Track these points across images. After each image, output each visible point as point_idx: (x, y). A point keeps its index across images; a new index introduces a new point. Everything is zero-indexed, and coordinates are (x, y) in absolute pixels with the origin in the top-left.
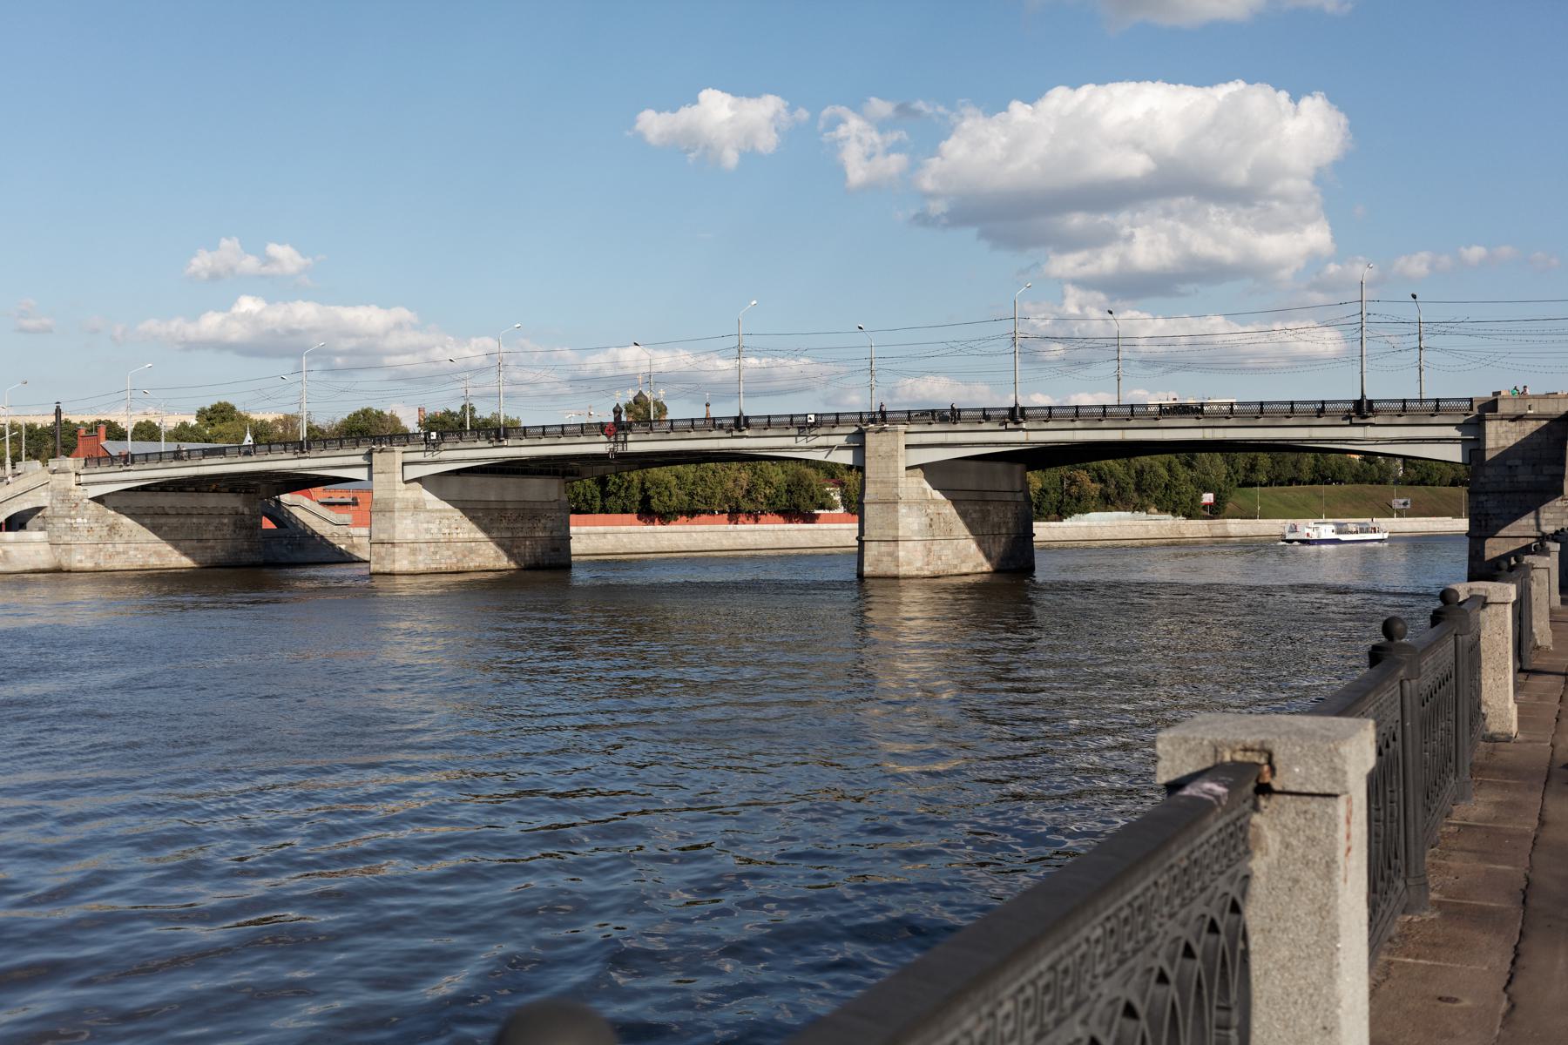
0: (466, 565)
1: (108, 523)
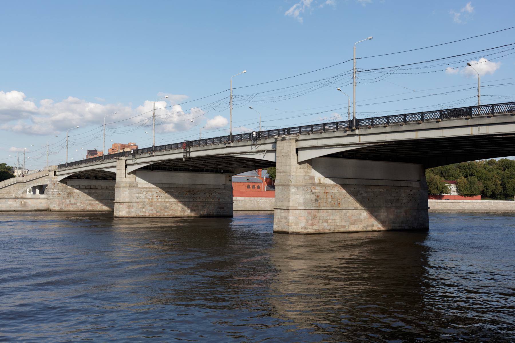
1: (68, 192)
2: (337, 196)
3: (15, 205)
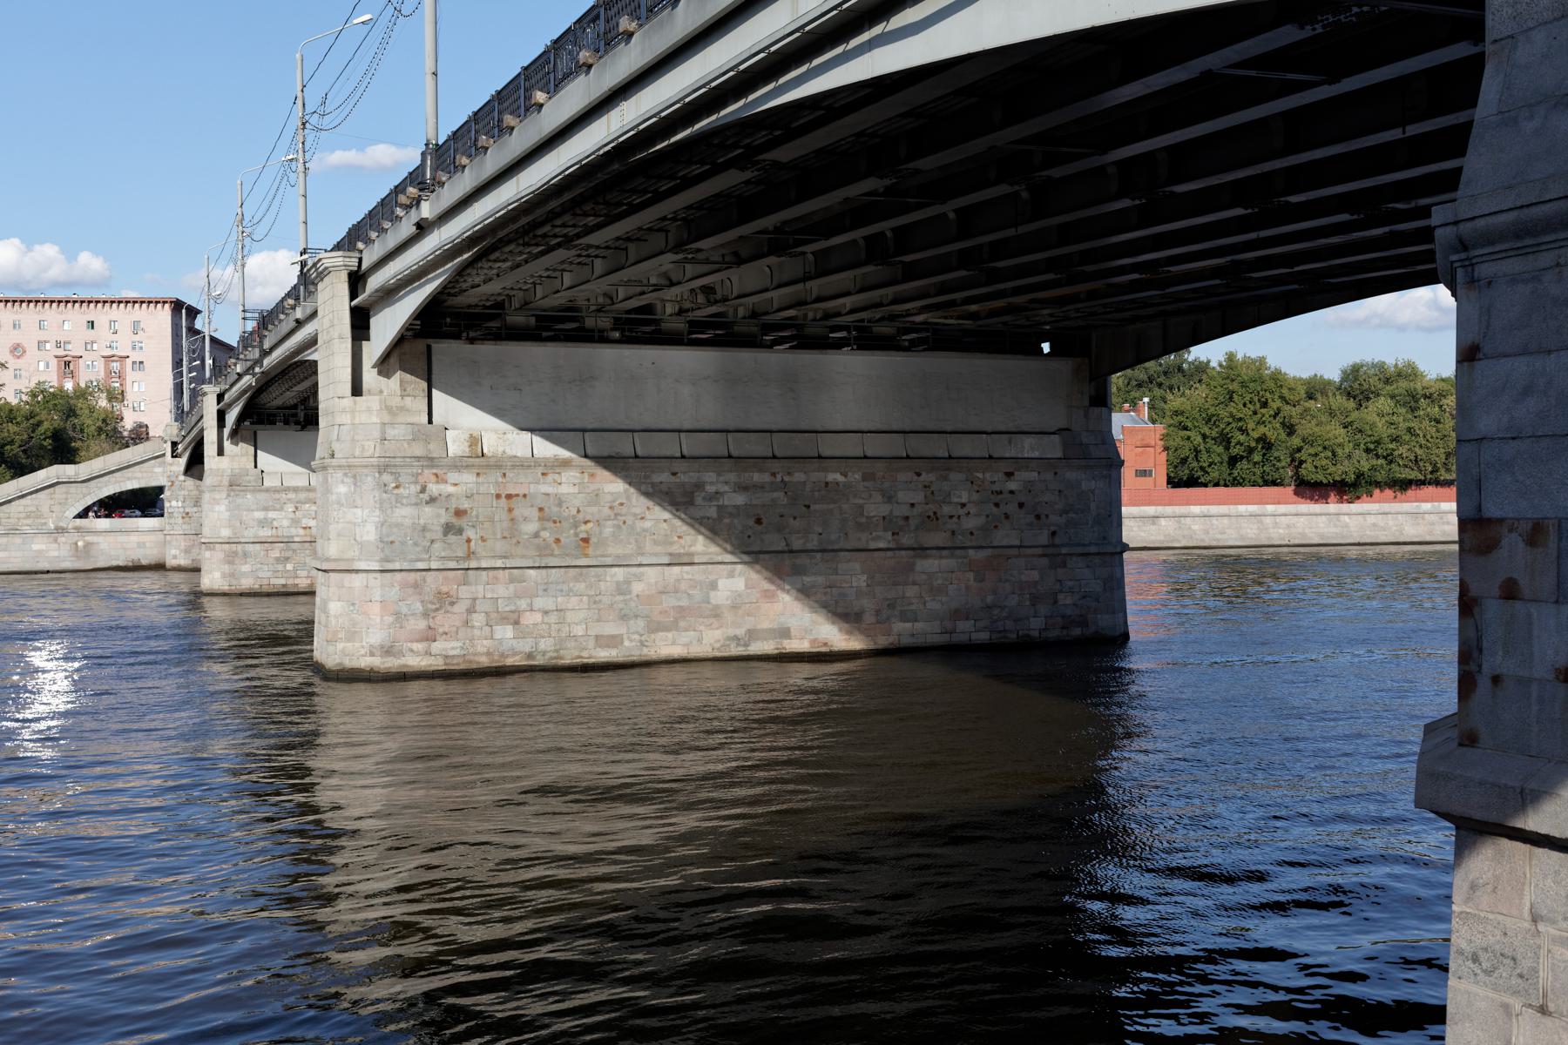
2: (574, 511)
3: (56, 554)
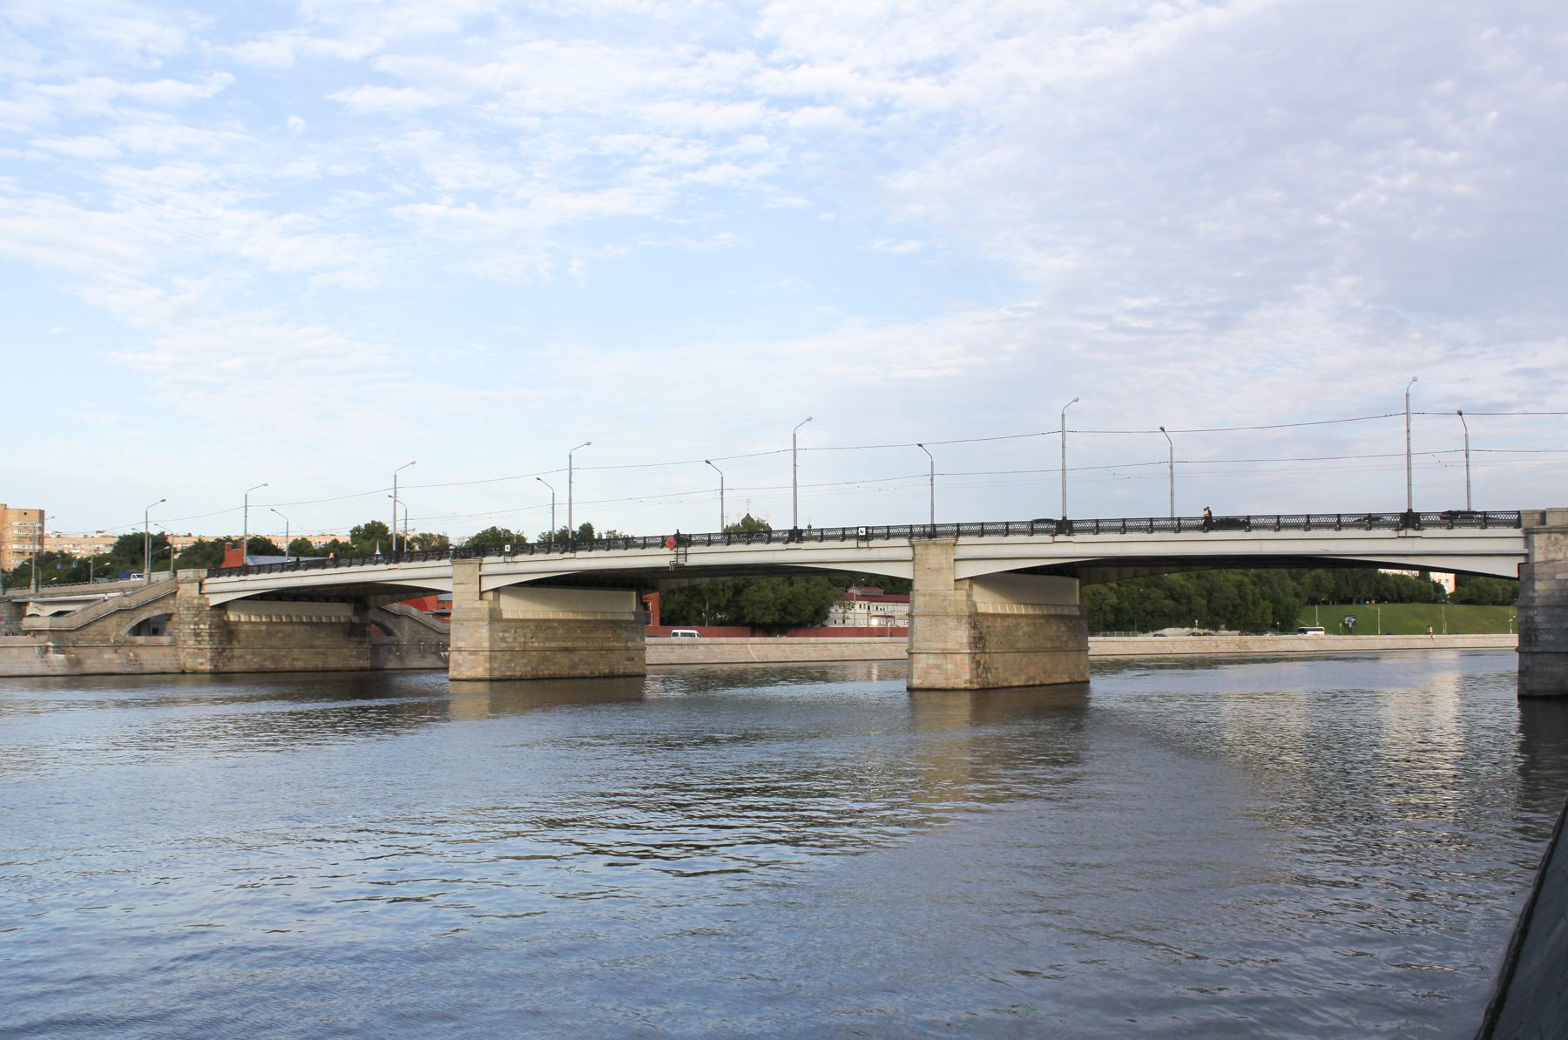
0: (540, 674)
